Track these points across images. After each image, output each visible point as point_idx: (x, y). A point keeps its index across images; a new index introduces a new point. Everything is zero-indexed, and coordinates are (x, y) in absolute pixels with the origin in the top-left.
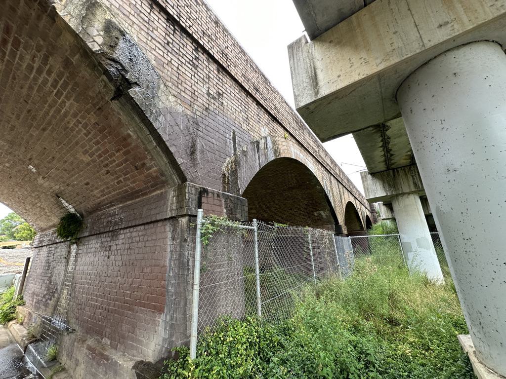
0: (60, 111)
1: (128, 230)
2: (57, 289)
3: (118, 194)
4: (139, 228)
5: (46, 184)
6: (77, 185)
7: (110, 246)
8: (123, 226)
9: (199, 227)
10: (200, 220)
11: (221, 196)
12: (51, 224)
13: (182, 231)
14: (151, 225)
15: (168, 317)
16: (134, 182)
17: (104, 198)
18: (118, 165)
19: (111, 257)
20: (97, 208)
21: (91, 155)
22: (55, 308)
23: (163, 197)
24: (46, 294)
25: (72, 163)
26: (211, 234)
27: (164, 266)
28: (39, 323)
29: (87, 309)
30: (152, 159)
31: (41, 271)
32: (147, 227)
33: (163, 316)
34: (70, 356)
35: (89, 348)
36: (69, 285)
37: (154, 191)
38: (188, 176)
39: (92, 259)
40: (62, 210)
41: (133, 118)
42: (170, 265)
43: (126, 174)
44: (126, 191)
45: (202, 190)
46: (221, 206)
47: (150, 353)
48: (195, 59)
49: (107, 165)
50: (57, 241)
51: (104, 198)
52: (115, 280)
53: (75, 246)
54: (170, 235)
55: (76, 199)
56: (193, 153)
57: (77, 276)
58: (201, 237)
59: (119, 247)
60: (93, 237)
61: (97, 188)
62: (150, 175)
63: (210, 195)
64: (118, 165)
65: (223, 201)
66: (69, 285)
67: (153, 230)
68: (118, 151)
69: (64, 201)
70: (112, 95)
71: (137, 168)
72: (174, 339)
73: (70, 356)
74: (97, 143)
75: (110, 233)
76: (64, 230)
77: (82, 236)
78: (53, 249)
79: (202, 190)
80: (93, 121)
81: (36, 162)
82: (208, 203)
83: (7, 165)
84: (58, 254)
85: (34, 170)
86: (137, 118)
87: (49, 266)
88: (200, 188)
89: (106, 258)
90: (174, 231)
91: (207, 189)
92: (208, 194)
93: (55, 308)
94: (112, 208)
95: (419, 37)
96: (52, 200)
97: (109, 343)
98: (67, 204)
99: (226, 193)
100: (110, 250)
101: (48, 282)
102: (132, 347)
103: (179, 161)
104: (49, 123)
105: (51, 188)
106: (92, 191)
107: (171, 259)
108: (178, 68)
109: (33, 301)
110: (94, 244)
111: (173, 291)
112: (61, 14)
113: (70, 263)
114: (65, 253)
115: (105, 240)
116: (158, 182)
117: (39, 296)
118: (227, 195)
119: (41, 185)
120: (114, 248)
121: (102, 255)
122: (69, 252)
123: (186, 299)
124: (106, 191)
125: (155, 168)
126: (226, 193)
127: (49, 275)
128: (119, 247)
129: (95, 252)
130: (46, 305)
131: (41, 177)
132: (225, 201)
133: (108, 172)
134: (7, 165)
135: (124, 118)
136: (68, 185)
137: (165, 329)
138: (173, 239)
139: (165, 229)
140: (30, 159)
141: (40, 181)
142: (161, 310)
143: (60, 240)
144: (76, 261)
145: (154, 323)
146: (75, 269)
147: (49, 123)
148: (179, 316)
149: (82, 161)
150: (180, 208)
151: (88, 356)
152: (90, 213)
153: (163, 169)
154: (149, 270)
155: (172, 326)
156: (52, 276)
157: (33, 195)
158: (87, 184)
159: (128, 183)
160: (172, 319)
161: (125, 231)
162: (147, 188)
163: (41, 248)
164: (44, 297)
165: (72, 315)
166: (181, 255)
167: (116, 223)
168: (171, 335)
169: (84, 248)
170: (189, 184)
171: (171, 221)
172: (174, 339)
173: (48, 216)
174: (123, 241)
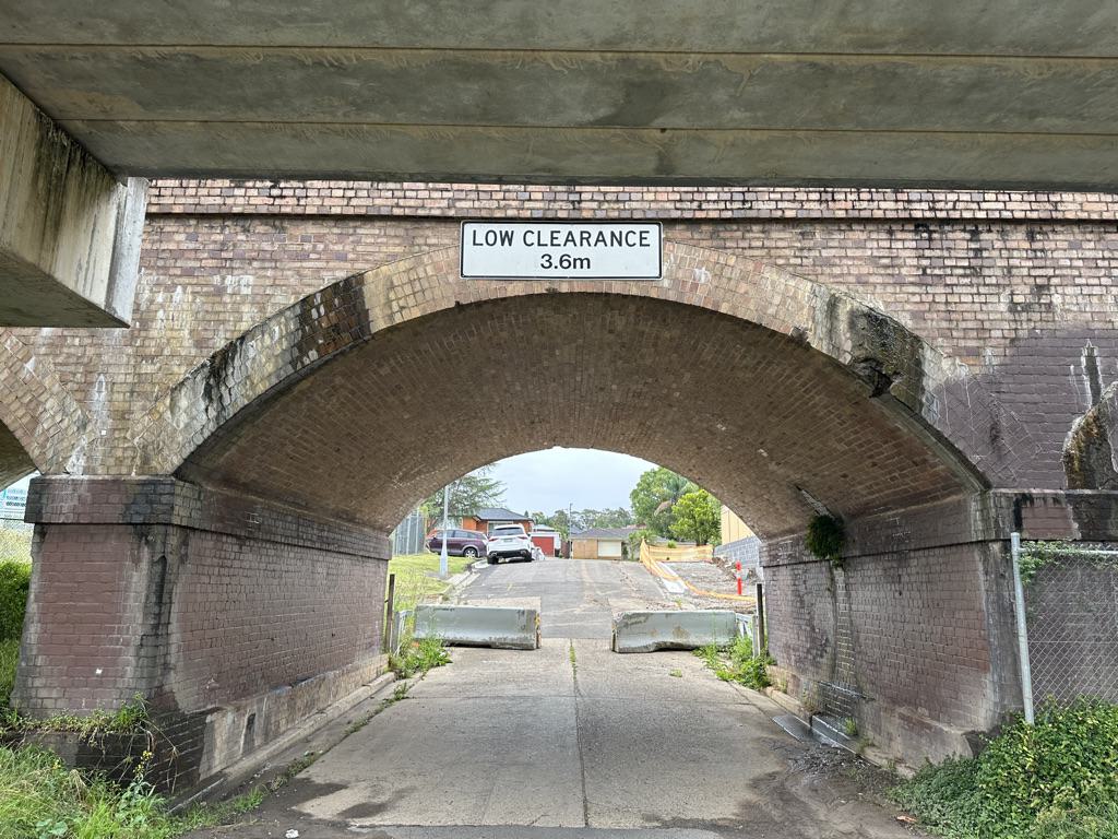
0: (807, 404)
1: (921, 553)
2: (827, 640)
3: (895, 493)
4: (937, 551)
5: (781, 471)
6: (829, 475)
7: (899, 576)
8: (913, 547)
9: (1015, 559)
10: (1016, 548)
11: (1064, 500)
12: (787, 527)
13: (996, 562)
14: (954, 549)
15: (996, 677)
16: (916, 480)
17: (874, 497)
18: (888, 458)
19: (904, 593)
20: (865, 510)
21: (847, 444)
22: (833, 668)
23: (961, 508)
24: (811, 648)
25: (821, 451)
26: (1033, 569)
27: (981, 611)
28: (815, 690)
29: (886, 669)
30: (935, 455)
31: (789, 609)
32: (948, 551)
33: (989, 676)
34: (877, 729)
35: (902, 717)
36: (846, 635)
37: (948, 495)
38: (992, 477)
39: (875, 595)
40: (805, 508)
41: (899, 413)
42: (988, 609)
43: (902, 469)
44: (906, 491)
45: (1020, 497)
46: (1066, 517)
47: (982, 721)
48: (975, 257)
49: (871, 457)
50: (805, 559)
51: (874, 497)
52: (917, 628)
53: (840, 571)
54: (981, 568)
55: (829, 494)
56: (995, 438)
57: (858, 622)
58: (1021, 573)
59: (913, 579)
60: (867, 559)
61: (860, 483)
62: (936, 474)
63: (1037, 502)
64: (888, 458)
65: (1070, 508)
66: (846, 635)
67: (957, 556)
68: (886, 442)
69: (807, 495)
70: (871, 393)
71: (916, 464)
72: (1006, 702)
73: (877, 729)
74: (856, 432)
75: (895, 556)
76: (820, 544)
77: (48, 223)
78: (800, 572)
79: (1020, 497)
80: (848, 412)
81: (770, 446)
82: (1034, 517)
83: (730, 447)
84: (812, 582)
85: (765, 454)
86: (903, 413)
87: (802, 602)
88: (1016, 494)
89: (897, 594)
90: (986, 561)
91: (1031, 495)
92: (1032, 502)
93: (833, 668)
94: (889, 513)
95: (591, 813)
96: (789, 492)
97: (927, 714)
98: (812, 500)
99: (1079, 491)
100: (900, 582)
101: (808, 628)
102: (959, 717)
103: (974, 459)
104: (793, 413)
105: (788, 476)
106: (853, 485)
107: (987, 601)
108: (947, 303)
109: (790, 660)
110: (871, 570)
111: (996, 643)
112: (814, 346)
113: (841, 598)
114: (826, 582)
115: (890, 564)
116: (950, 485)
117: (798, 650)
118: (1081, 496)
119: (773, 472)
120: (905, 579)
121: (886, 593)
122: (832, 580)
123: (1015, 655)
124: (875, 488)
125: (942, 467)
126: (1079, 491)
127: (807, 617)
128: (913, 579)
129: (877, 583)
130: (816, 664)
131: (774, 463)
132: (1075, 508)
133: (874, 465)
134: (730, 447)
135: (886, 411)
136: (815, 475)
137: (995, 691)
138: (986, 573)
139: (973, 557)
140: (762, 443)
141: (772, 466)
142: (985, 669)
143: (814, 558)
144: (848, 595)
145: (981, 686)
146: (851, 609)
147: (793, 413)
148: (1007, 674)
149: (835, 450)
150: (986, 530)
151: (903, 727)
152: (853, 516)
153: (954, 468)
154: (961, 615)
155: (1001, 687)
156: (812, 618)
157: (759, 483)
158: (845, 476)
159: (907, 480)
160: (1000, 678)
161: (917, 554)
162: (937, 490)
163: (775, 569)
164: (808, 651)
165: (864, 679)
166: (1000, 596)
167: (901, 541)
168: (1002, 699)
169: (857, 577)
170: (995, 494)
171: (980, 545)
172: (1006, 702)
173: (782, 515)
174: (918, 569)
